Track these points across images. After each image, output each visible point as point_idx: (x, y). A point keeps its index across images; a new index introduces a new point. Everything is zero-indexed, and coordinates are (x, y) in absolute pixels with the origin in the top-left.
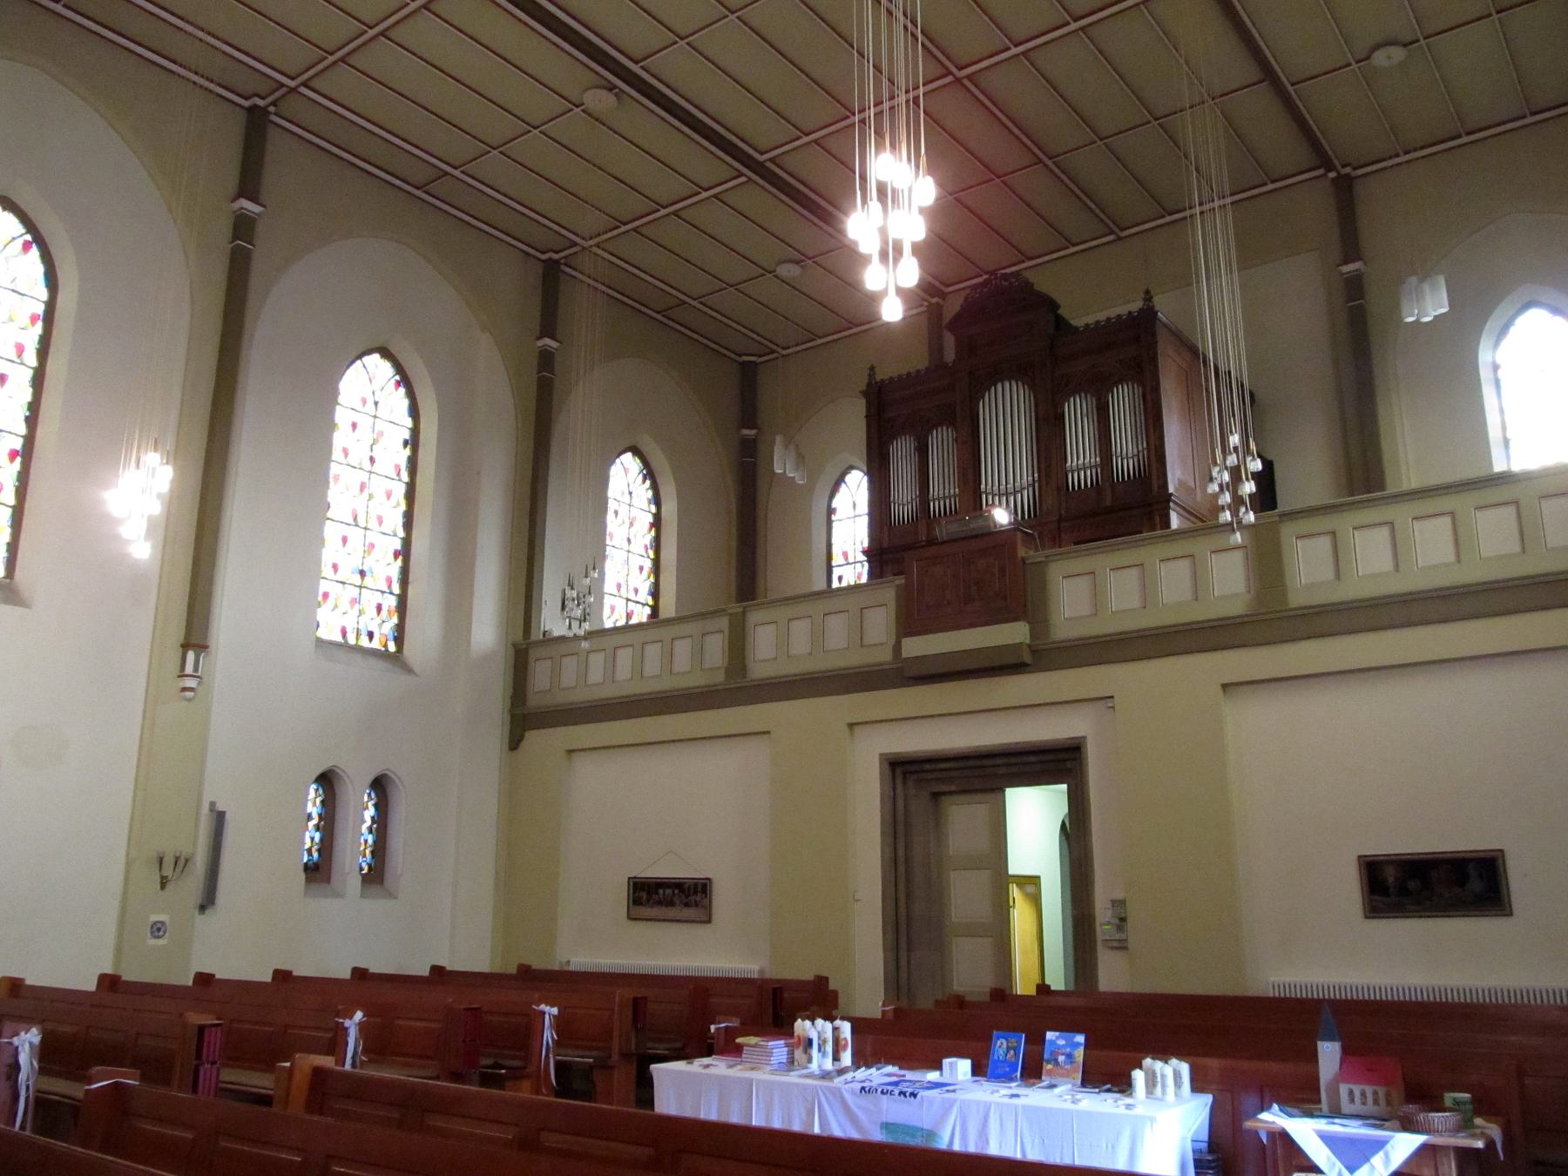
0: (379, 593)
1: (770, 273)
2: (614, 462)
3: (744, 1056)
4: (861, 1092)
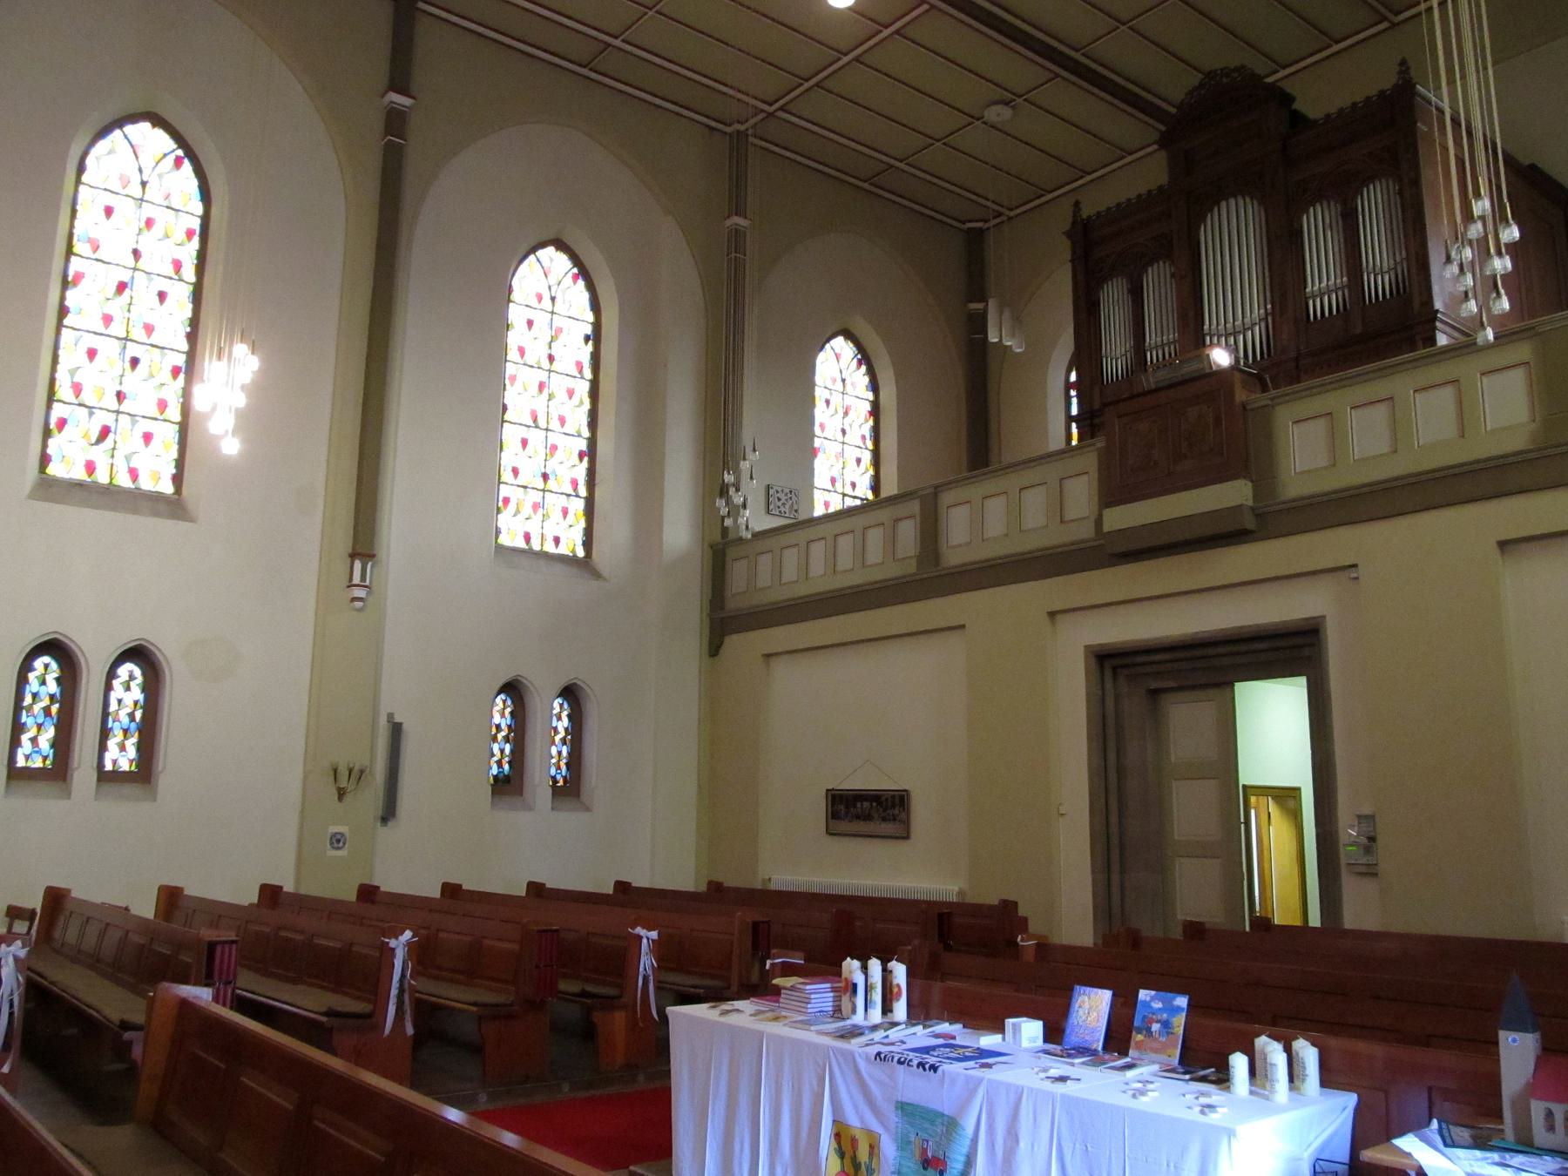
0: (564, 496)
1: (978, 119)
2: (822, 348)
3: (781, 1000)
4: (876, 1059)
